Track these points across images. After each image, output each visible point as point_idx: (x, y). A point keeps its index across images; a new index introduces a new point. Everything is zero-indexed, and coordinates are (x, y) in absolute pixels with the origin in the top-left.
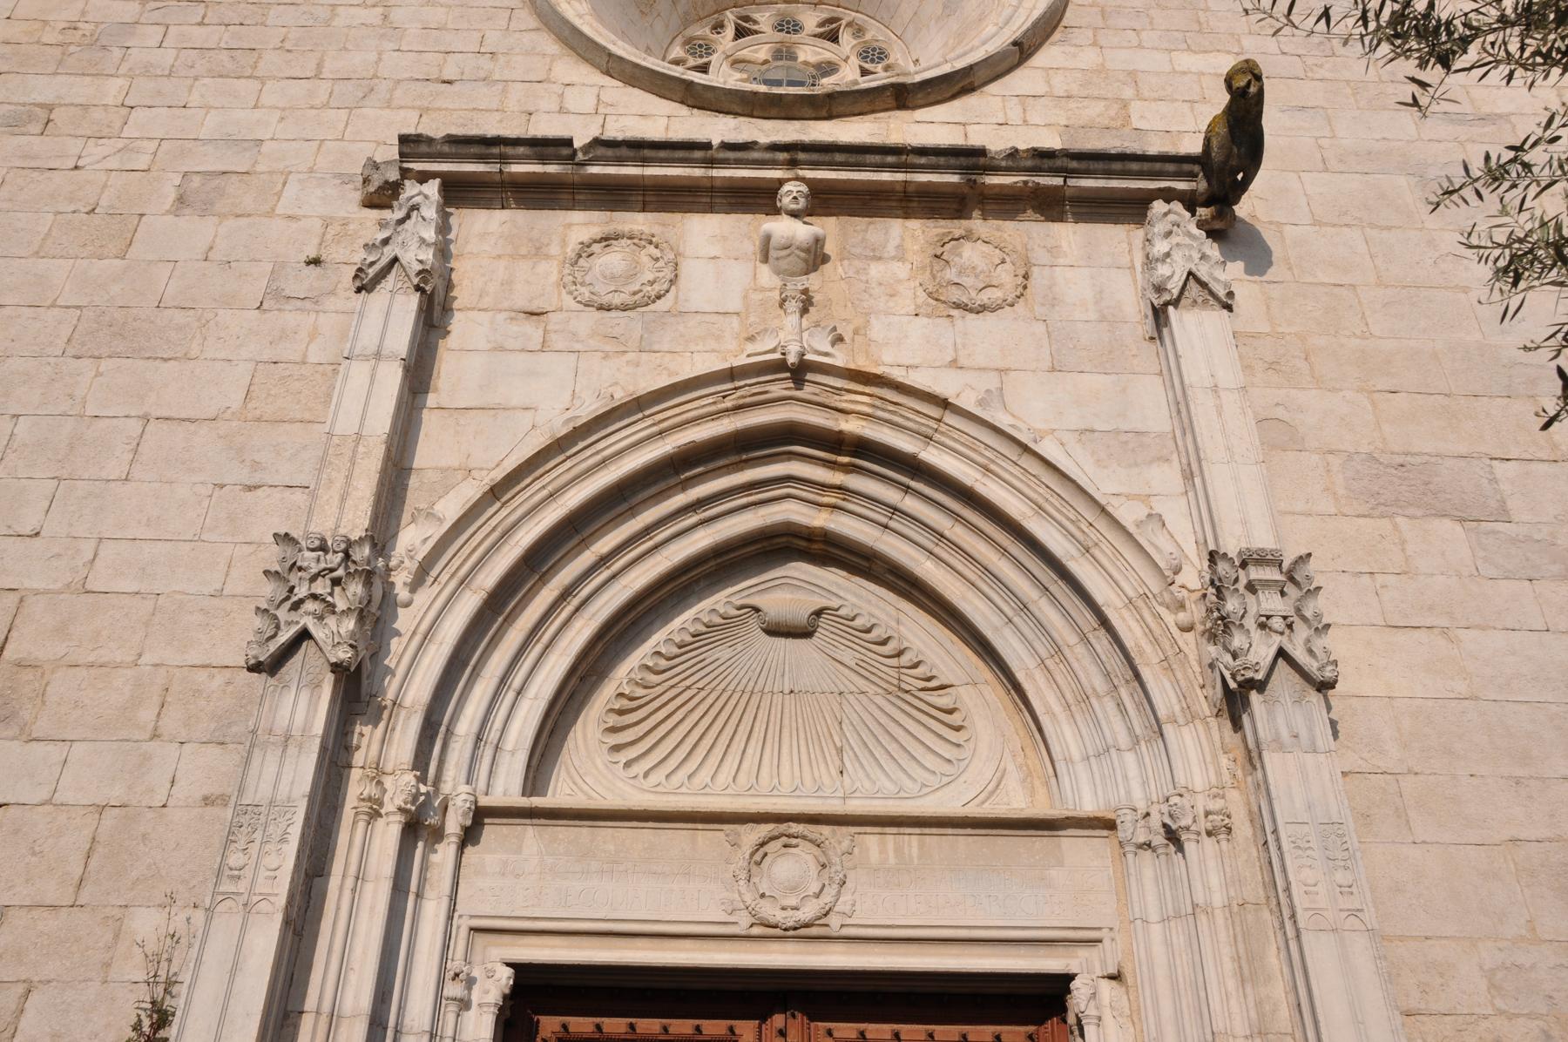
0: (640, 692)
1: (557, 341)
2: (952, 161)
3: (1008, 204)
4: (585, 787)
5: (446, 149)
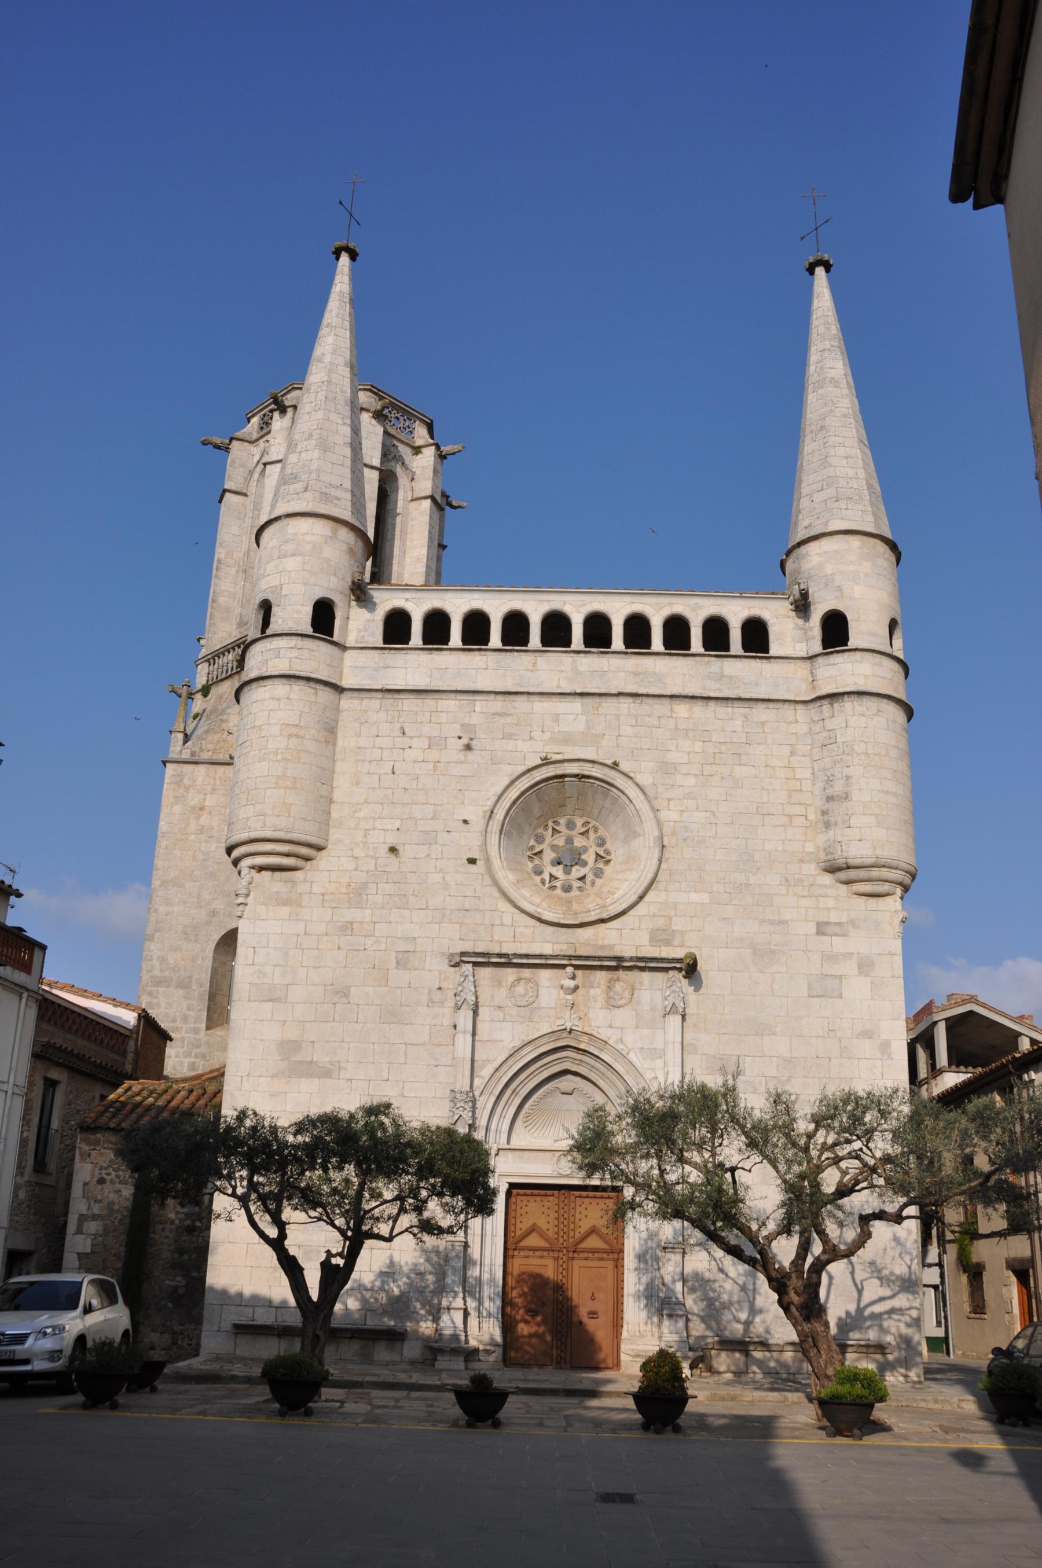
1: (508, 1018)
3: (630, 968)
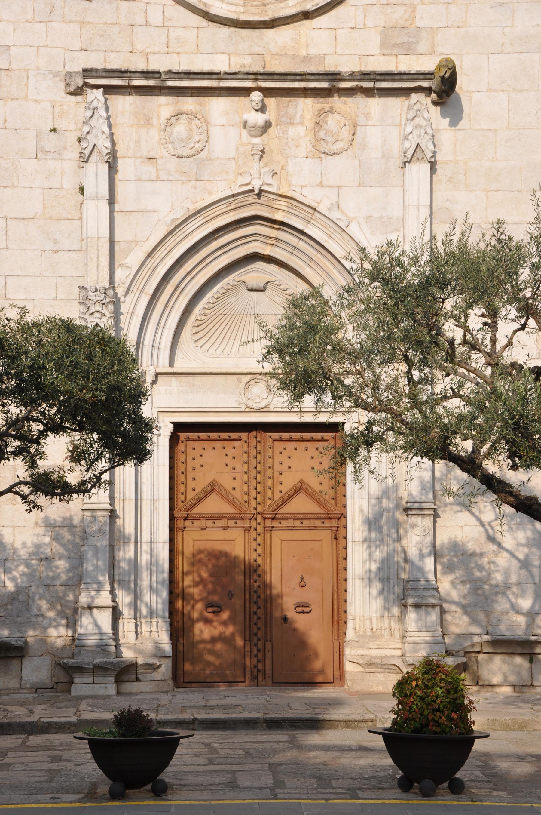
0: (203, 318)
2: (325, 77)
4: (188, 356)
5: (104, 74)
